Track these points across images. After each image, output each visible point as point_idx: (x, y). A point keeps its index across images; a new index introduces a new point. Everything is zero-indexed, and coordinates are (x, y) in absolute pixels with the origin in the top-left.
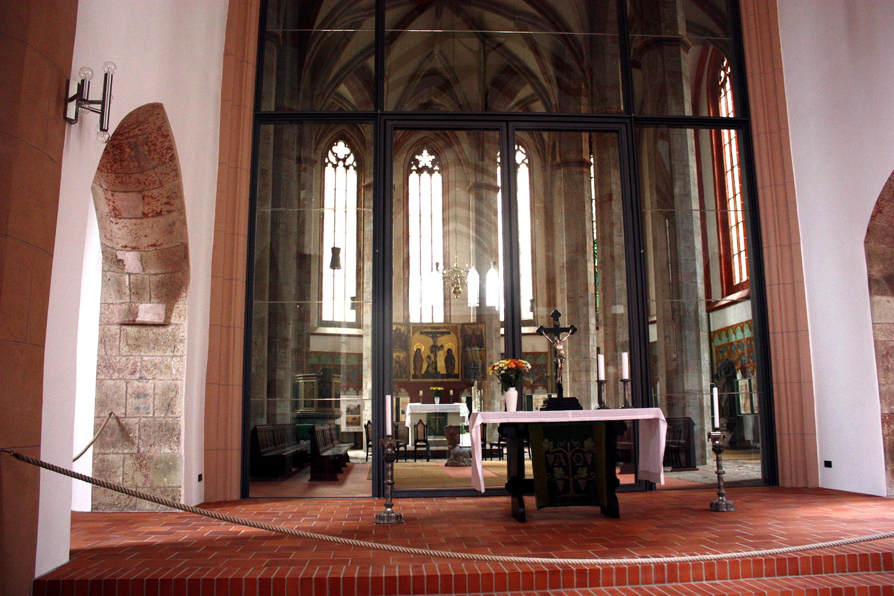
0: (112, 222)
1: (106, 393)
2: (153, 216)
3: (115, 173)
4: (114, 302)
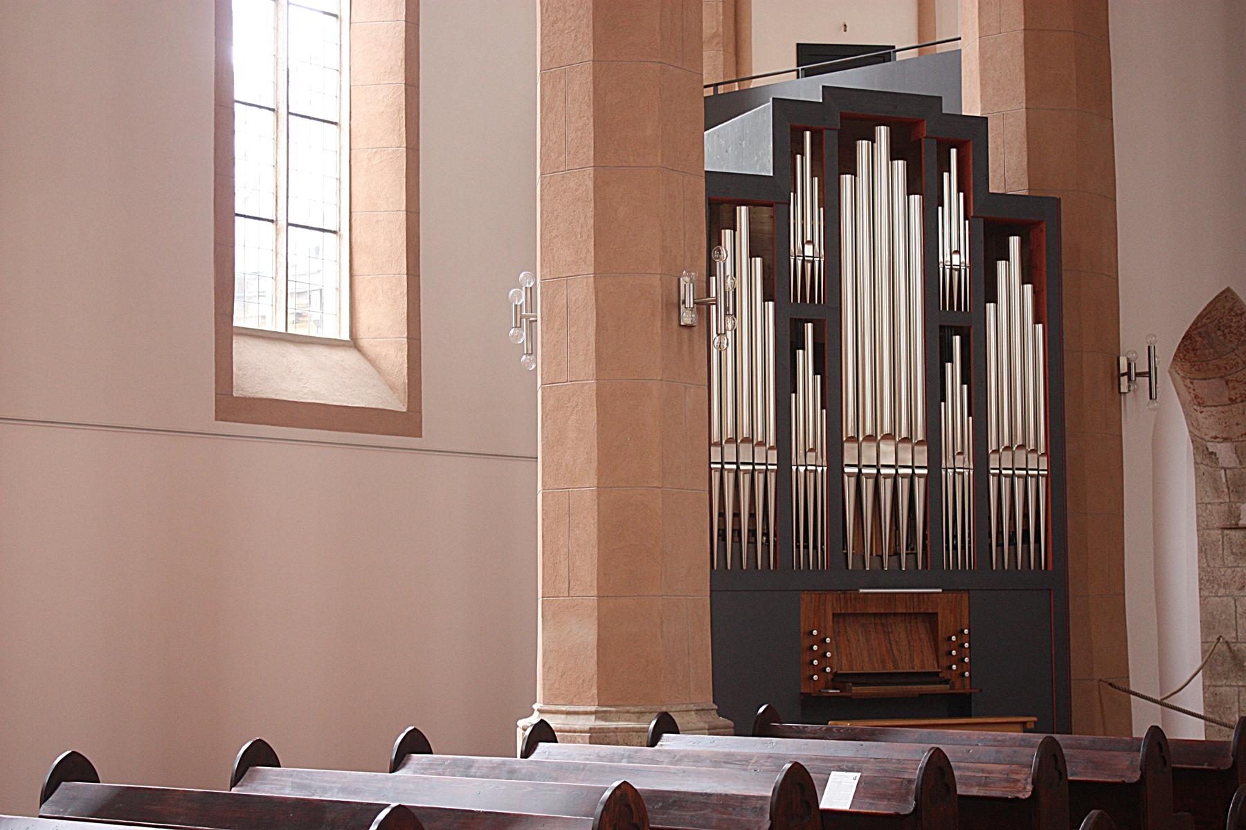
0: (1196, 411)
1: (1212, 614)
3: (1190, 362)
4: (1212, 501)
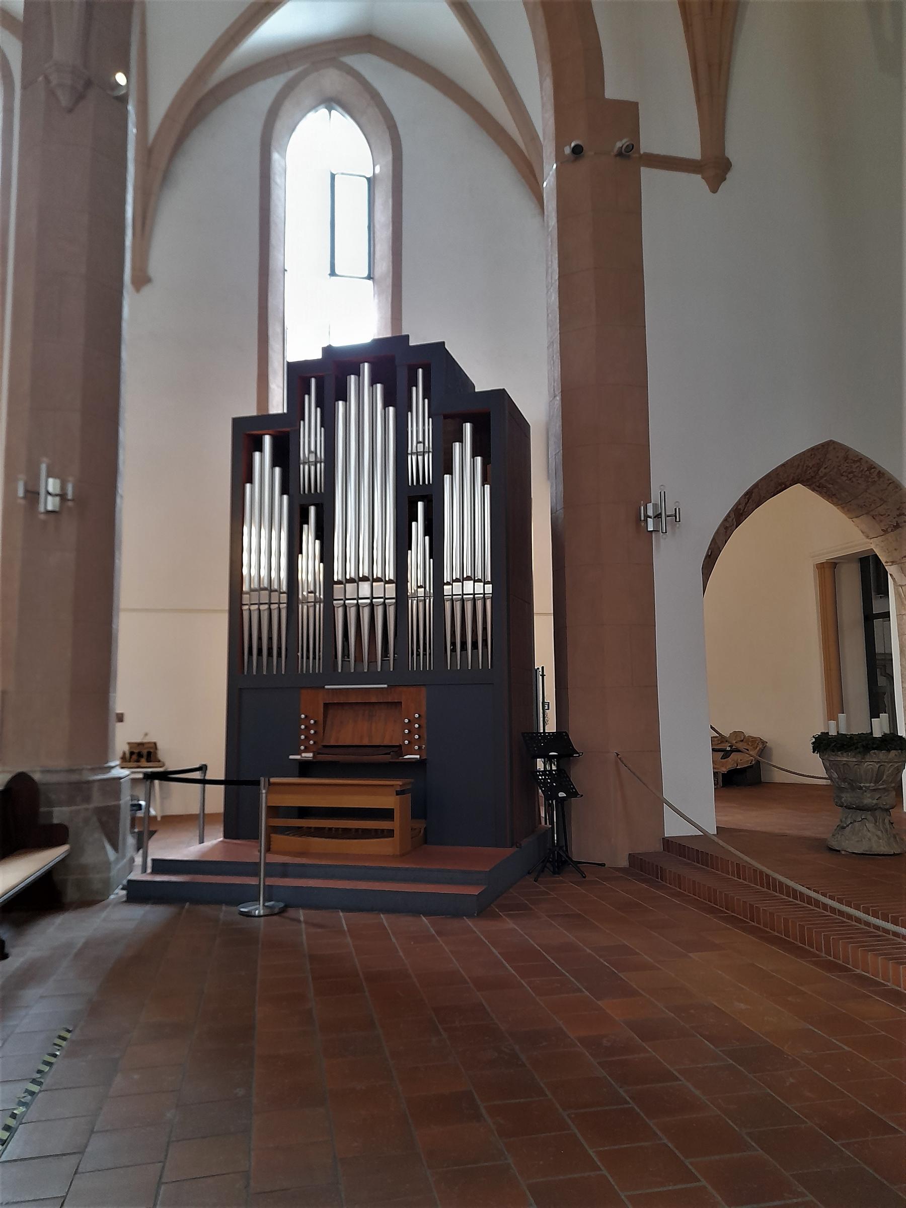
2: (892, 531)
